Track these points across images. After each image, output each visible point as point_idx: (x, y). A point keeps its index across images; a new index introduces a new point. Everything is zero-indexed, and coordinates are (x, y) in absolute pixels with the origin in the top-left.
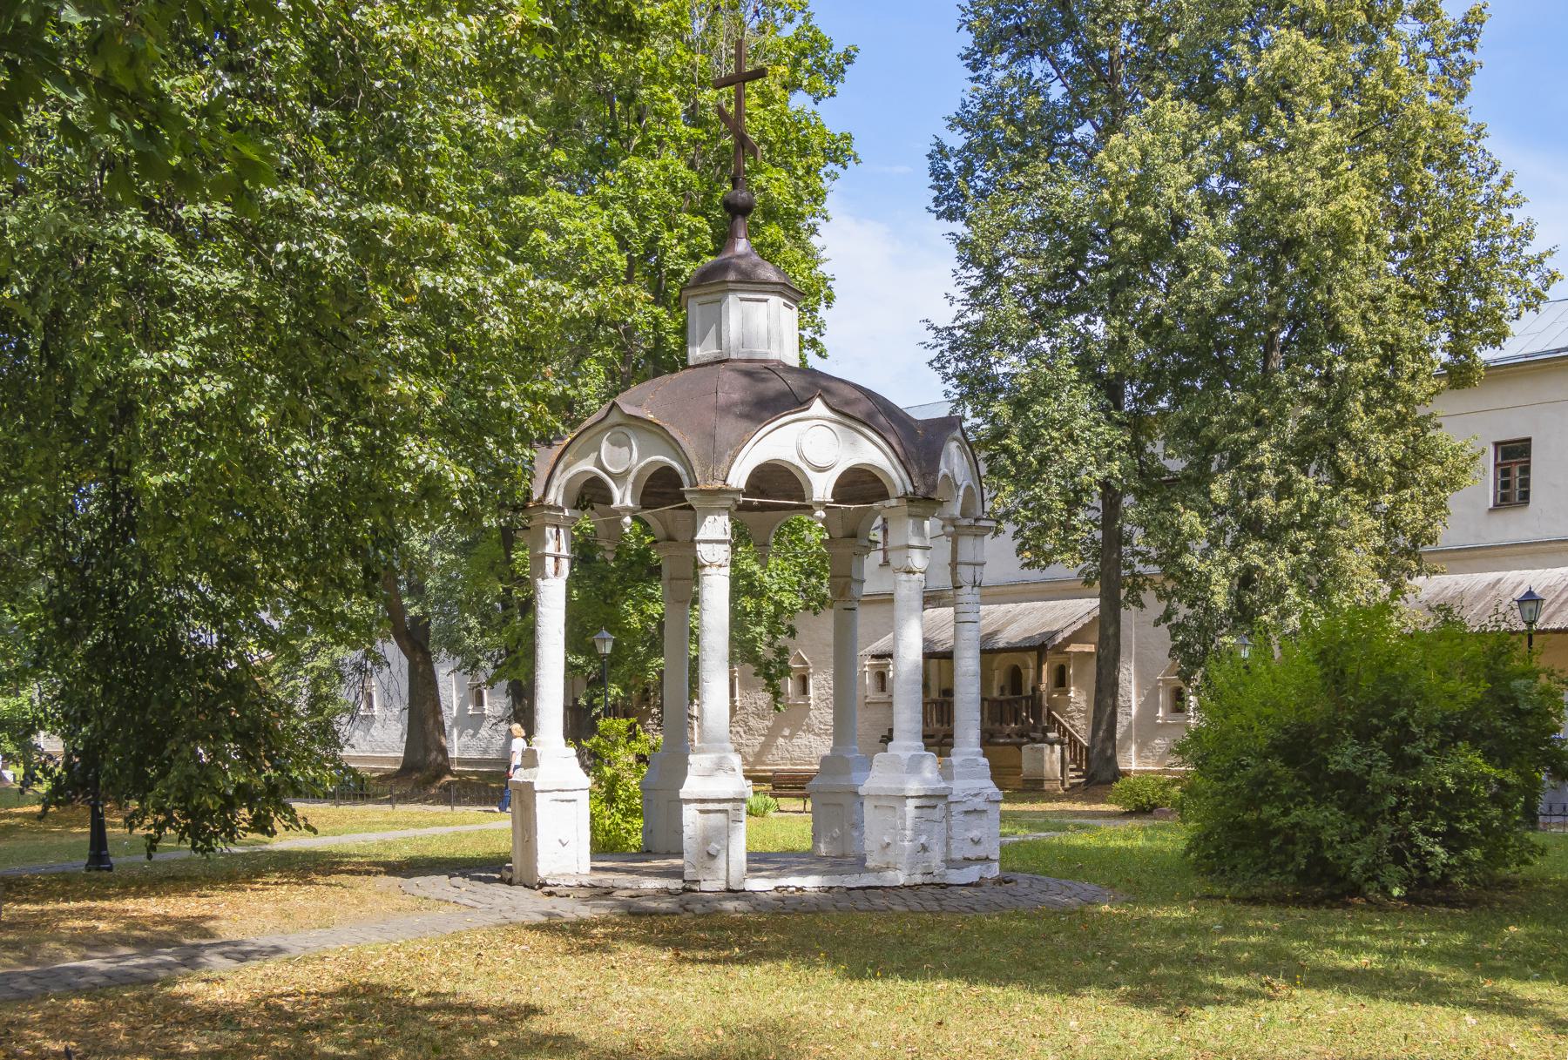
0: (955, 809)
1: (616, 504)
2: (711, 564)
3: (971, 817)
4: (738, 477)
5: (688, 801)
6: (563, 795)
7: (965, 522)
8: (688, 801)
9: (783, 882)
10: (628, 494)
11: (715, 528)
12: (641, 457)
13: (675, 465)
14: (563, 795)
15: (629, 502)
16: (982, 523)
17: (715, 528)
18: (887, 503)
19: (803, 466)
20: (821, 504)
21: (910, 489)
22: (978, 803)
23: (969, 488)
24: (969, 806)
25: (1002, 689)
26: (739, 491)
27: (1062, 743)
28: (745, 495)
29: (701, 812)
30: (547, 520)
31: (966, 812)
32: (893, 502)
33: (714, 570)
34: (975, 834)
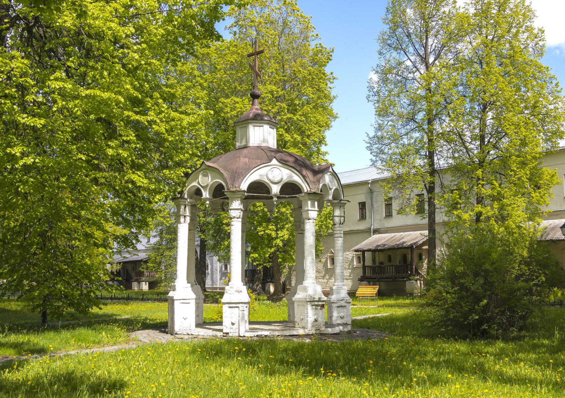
0: (334, 305)
1: (204, 196)
2: (234, 217)
3: (340, 309)
4: (244, 186)
5: (224, 303)
6: (185, 301)
7: (336, 201)
8: (224, 303)
9: (101, 350)
10: (208, 193)
11: (236, 205)
12: (212, 180)
13: (222, 182)
14: (185, 301)
15: (208, 196)
16: (342, 202)
17: (236, 205)
18: (301, 195)
19: (268, 182)
20: (275, 195)
21: (309, 189)
22: (343, 303)
23: (336, 189)
24: (339, 304)
25: (400, 262)
26: (244, 191)
27: (420, 280)
28: (247, 192)
29: (230, 307)
30: (181, 203)
31: (338, 307)
32: (303, 194)
33: (235, 219)
34: (342, 314)
